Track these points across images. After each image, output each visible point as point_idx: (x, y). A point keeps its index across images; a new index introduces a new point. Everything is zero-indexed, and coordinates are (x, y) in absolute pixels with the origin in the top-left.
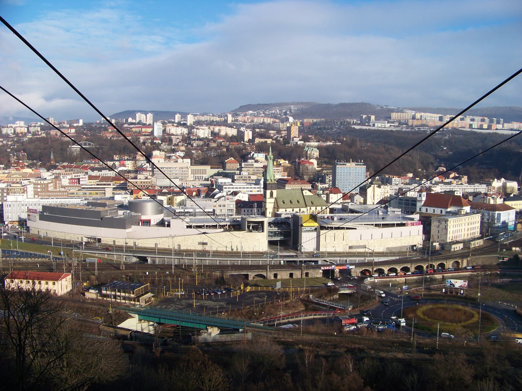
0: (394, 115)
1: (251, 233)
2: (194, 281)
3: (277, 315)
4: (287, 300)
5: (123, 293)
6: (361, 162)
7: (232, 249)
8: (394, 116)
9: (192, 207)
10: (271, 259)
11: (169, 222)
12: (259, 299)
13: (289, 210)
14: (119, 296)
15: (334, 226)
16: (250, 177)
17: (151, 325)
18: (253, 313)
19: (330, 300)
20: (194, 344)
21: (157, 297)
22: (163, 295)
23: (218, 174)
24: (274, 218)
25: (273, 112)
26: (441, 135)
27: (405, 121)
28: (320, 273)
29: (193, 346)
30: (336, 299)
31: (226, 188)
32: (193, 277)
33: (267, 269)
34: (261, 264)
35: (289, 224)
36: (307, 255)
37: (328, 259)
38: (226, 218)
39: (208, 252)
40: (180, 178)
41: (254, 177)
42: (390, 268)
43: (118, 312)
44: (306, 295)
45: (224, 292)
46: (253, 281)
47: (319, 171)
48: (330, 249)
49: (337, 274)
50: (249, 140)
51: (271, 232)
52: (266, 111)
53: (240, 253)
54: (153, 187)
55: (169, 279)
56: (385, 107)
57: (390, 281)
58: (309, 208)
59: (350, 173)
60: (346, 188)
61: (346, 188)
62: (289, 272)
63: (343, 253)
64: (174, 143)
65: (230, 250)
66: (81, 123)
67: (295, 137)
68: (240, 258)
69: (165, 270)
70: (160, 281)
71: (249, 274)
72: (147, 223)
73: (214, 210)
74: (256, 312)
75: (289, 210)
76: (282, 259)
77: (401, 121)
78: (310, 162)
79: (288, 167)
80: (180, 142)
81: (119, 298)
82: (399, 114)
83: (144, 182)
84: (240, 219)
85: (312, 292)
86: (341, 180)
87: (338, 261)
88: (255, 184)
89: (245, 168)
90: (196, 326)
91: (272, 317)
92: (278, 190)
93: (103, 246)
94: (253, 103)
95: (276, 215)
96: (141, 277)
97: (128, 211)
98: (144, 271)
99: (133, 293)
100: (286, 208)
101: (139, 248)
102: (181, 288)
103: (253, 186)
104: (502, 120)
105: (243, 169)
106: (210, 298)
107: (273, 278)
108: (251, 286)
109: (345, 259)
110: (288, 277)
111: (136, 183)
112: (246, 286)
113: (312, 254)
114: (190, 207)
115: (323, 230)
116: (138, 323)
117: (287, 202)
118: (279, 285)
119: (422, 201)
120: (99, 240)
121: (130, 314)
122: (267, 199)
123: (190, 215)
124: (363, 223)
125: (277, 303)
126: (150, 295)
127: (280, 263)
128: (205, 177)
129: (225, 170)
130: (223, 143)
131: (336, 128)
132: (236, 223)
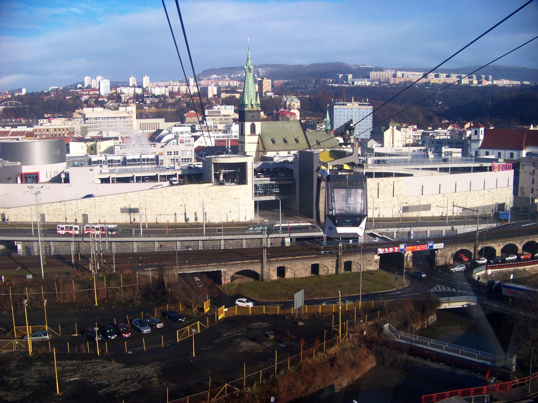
0: (373, 74)
1: (222, 187)
2: (91, 294)
4: (330, 345)
6: (365, 102)
7: (187, 220)
8: (373, 74)
11: (67, 175)
12: (252, 344)
24: (261, 163)
25: (240, 75)
26: (433, 89)
27: (385, 80)
28: (376, 261)
34: (244, 246)
35: (291, 171)
39: (137, 226)
42: (505, 244)
44: (370, 323)
45: (159, 326)
46: (232, 285)
50: (214, 95)
52: (231, 75)
53: (201, 225)
56: (362, 66)
57: (510, 273)
62: (310, 263)
64: (123, 101)
65: (183, 221)
66: (24, 92)
67: (268, 92)
68: (202, 235)
71: (222, 270)
72: (34, 178)
76: (287, 235)
77: (381, 80)
78: (291, 113)
80: (130, 99)
82: (379, 72)
94: (216, 67)
104: (490, 77)
109: (407, 229)
110: (307, 273)
111: (48, 130)
117: (279, 141)
119: (480, 140)
122: (246, 137)
124: (421, 167)
127: (283, 242)
130: (182, 99)
131: (312, 87)
132: (192, 172)
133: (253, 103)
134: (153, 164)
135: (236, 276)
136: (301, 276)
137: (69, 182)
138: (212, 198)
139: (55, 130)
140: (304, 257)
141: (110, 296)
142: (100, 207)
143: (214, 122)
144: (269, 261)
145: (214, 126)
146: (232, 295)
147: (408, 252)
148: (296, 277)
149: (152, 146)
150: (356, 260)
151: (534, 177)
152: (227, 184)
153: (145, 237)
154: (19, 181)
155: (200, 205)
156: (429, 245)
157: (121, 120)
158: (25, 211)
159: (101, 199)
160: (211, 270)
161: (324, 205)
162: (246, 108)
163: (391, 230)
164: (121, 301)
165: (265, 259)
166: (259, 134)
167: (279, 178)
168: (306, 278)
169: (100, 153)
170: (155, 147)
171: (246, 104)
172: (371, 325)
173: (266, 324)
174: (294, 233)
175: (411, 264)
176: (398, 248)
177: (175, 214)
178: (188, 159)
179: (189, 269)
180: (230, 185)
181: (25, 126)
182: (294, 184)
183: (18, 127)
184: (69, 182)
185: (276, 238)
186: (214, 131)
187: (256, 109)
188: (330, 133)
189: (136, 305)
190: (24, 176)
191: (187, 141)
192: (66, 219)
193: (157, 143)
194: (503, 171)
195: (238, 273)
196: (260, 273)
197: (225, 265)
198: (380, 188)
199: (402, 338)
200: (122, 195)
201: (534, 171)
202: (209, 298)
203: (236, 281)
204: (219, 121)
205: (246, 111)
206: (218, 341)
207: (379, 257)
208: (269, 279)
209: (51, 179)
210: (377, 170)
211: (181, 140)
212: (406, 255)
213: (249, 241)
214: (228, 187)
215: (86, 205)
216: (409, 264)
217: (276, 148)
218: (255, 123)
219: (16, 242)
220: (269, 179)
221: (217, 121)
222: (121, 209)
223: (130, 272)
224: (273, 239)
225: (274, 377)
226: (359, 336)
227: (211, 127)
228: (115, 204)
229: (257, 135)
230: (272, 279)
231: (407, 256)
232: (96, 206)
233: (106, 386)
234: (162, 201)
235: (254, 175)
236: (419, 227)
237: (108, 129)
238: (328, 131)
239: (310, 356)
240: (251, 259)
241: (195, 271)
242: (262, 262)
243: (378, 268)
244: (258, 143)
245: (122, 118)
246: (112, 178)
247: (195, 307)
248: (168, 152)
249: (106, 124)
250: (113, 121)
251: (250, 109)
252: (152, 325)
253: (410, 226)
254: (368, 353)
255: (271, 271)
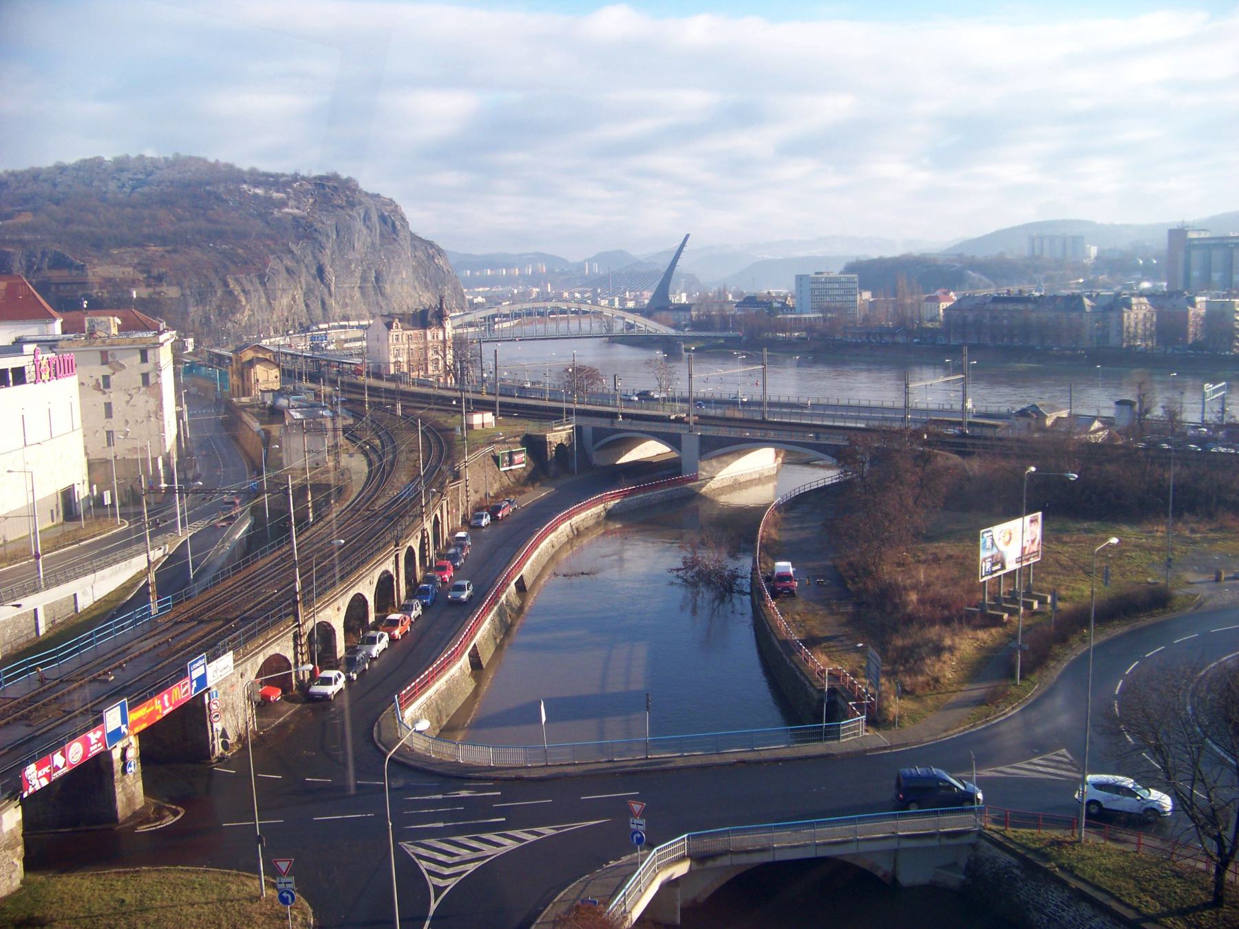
151: (109, 397)
161: (722, 428)
176: (99, 734)
194: (59, 380)
201: (106, 378)
222: (106, 417)
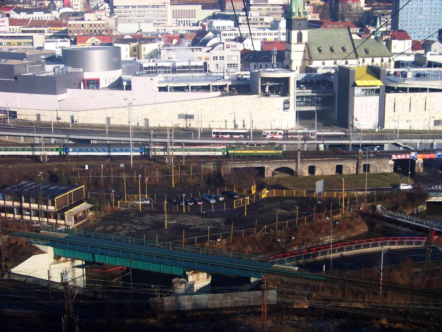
1: (267, 98)
3: (319, 241)
4: (336, 213)
5: (36, 203)
9: (170, 60)
10: (303, 142)
11: (129, 82)
13: (330, 63)
14: (29, 210)
15: (408, 86)
16: (262, 19)
17: (79, 267)
18: (275, 240)
19: (412, 214)
20: (154, 316)
21: (100, 210)
22: (111, 205)
23: (215, 17)
24: (304, 75)
28: (390, 165)
29: (152, 321)
30: (423, 211)
31: (225, 35)
32: (168, 172)
33: (296, 158)
35: (330, 85)
36: (365, 134)
37: (400, 142)
38: (226, 74)
39: (195, 131)
40: (155, 21)
41: (269, 19)
43: (13, 241)
44: (369, 205)
45: (221, 199)
46: (273, 178)
47: (367, 13)
48: (404, 126)
49: (419, 168)
51: (302, 97)
54: (109, 32)
55: (124, 176)
58: (361, 60)
59: (421, 9)
60: (415, 33)
61: (415, 33)
63: (424, 132)
69: (119, 161)
70: (107, 180)
71: (266, 166)
73: (205, 64)
74: (281, 237)
75: (330, 63)
76: (321, 142)
79: (320, 7)
81: (28, 213)
83: (95, 25)
84: (249, 77)
85: (380, 199)
86: (406, 21)
87: (418, 145)
88: (271, 29)
89: (255, 5)
90: (165, 269)
91: (309, 245)
92: (310, 30)
93: (20, 123)
95: (307, 70)
96: (75, 174)
97: (62, 66)
98: (82, 163)
99: (53, 205)
100: (324, 60)
101: (77, 126)
102: (143, 193)
103: (268, 31)
105: (251, 7)
106: (195, 211)
107: (306, 173)
108: (270, 188)
109: (430, 141)
110: (333, 172)
111: (83, 26)
112: (260, 188)
113: (369, 133)
114: (167, 59)
115: (389, 92)
116: (54, 263)
117: (326, 49)
118: (319, 186)
120: (13, 114)
121: (38, 246)
123: (165, 72)
125: (319, 220)
126: (84, 206)
127: (318, 148)
128: (193, 22)
129: (224, 11)
132: (241, 83)
133: (300, 11)
134: (201, 71)
135: (276, 172)
136: (328, 174)
137: (131, 90)
138: (258, 108)
139: (91, 25)
140: (330, 159)
141: (183, 181)
142: (160, 113)
143: (260, 13)
144: (302, 161)
145: (260, 19)
146: (272, 185)
147: (420, 159)
148: (323, 174)
149: (198, 50)
150: (374, 164)
152: (272, 96)
153: (202, 139)
154: (82, 87)
155: (247, 114)
156: (438, 154)
157: (153, 9)
158: (92, 114)
159: (161, 106)
160: (257, 166)
162: (294, 16)
163: (414, 141)
164: (191, 185)
165: (299, 159)
166: (306, 42)
167: (319, 90)
168: (332, 176)
169: (145, 55)
170: (200, 51)
171: (294, 13)
172: (369, 206)
173: (294, 202)
174: (326, 140)
175: (422, 170)
176: (409, 155)
177: (226, 121)
178: (234, 64)
179: (240, 165)
180: (274, 97)
181: (41, 11)
182: (334, 96)
183: (34, 12)
184: (131, 90)
185: (311, 144)
186: (259, 24)
187: (303, 18)
188: (380, 40)
189: (202, 188)
190: (86, 82)
191: (234, 46)
192: (129, 122)
193: (202, 47)
195: (277, 170)
196: (295, 170)
197: (268, 163)
198: (412, 102)
199: (388, 214)
200: (180, 103)
202: (255, 184)
203: (276, 176)
204: (266, 11)
205: (294, 19)
206: (261, 209)
207: (393, 162)
208: (302, 175)
209: (109, 85)
210: (407, 85)
211: (227, 45)
212: (417, 161)
213: (289, 146)
214: (273, 98)
215: (148, 110)
216: (420, 170)
217: (323, 58)
218: (302, 31)
219: (91, 141)
220: (310, 91)
221: (263, 11)
222: (178, 115)
223: (196, 165)
224: (309, 145)
225: (295, 227)
226: (357, 210)
227: (257, 19)
228: (174, 111)
229: (304, 43)
230: (305, 175)
231: (418, 163)
232: (157, 112)
233: (193, 226)
234: (215, 109)
235: (297, 87)
236: (440, 139)
237: (138, 19)
238: (378, 39)
239: (321, 218)
240: (288, 159)
241: (244, 167)
242: (297, 161)
243: (393, 171)
244: (304, 51)
245: (155, 7)
246: (170, 87)
247: (245, 190)
248: (214, 57)
249: (137, 13)
250: (144, 10)
251: (297, 18)
252: (217, 198)
253: (433, 138)
254: (362, 221)
255: (304, 169)
